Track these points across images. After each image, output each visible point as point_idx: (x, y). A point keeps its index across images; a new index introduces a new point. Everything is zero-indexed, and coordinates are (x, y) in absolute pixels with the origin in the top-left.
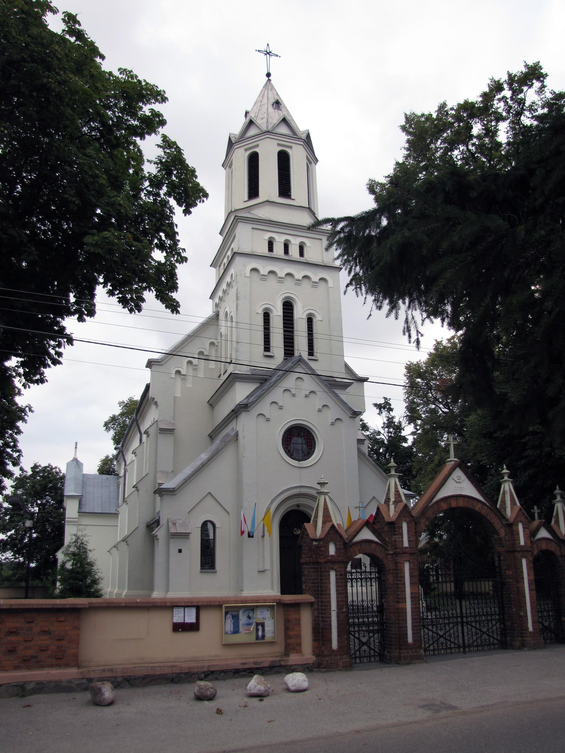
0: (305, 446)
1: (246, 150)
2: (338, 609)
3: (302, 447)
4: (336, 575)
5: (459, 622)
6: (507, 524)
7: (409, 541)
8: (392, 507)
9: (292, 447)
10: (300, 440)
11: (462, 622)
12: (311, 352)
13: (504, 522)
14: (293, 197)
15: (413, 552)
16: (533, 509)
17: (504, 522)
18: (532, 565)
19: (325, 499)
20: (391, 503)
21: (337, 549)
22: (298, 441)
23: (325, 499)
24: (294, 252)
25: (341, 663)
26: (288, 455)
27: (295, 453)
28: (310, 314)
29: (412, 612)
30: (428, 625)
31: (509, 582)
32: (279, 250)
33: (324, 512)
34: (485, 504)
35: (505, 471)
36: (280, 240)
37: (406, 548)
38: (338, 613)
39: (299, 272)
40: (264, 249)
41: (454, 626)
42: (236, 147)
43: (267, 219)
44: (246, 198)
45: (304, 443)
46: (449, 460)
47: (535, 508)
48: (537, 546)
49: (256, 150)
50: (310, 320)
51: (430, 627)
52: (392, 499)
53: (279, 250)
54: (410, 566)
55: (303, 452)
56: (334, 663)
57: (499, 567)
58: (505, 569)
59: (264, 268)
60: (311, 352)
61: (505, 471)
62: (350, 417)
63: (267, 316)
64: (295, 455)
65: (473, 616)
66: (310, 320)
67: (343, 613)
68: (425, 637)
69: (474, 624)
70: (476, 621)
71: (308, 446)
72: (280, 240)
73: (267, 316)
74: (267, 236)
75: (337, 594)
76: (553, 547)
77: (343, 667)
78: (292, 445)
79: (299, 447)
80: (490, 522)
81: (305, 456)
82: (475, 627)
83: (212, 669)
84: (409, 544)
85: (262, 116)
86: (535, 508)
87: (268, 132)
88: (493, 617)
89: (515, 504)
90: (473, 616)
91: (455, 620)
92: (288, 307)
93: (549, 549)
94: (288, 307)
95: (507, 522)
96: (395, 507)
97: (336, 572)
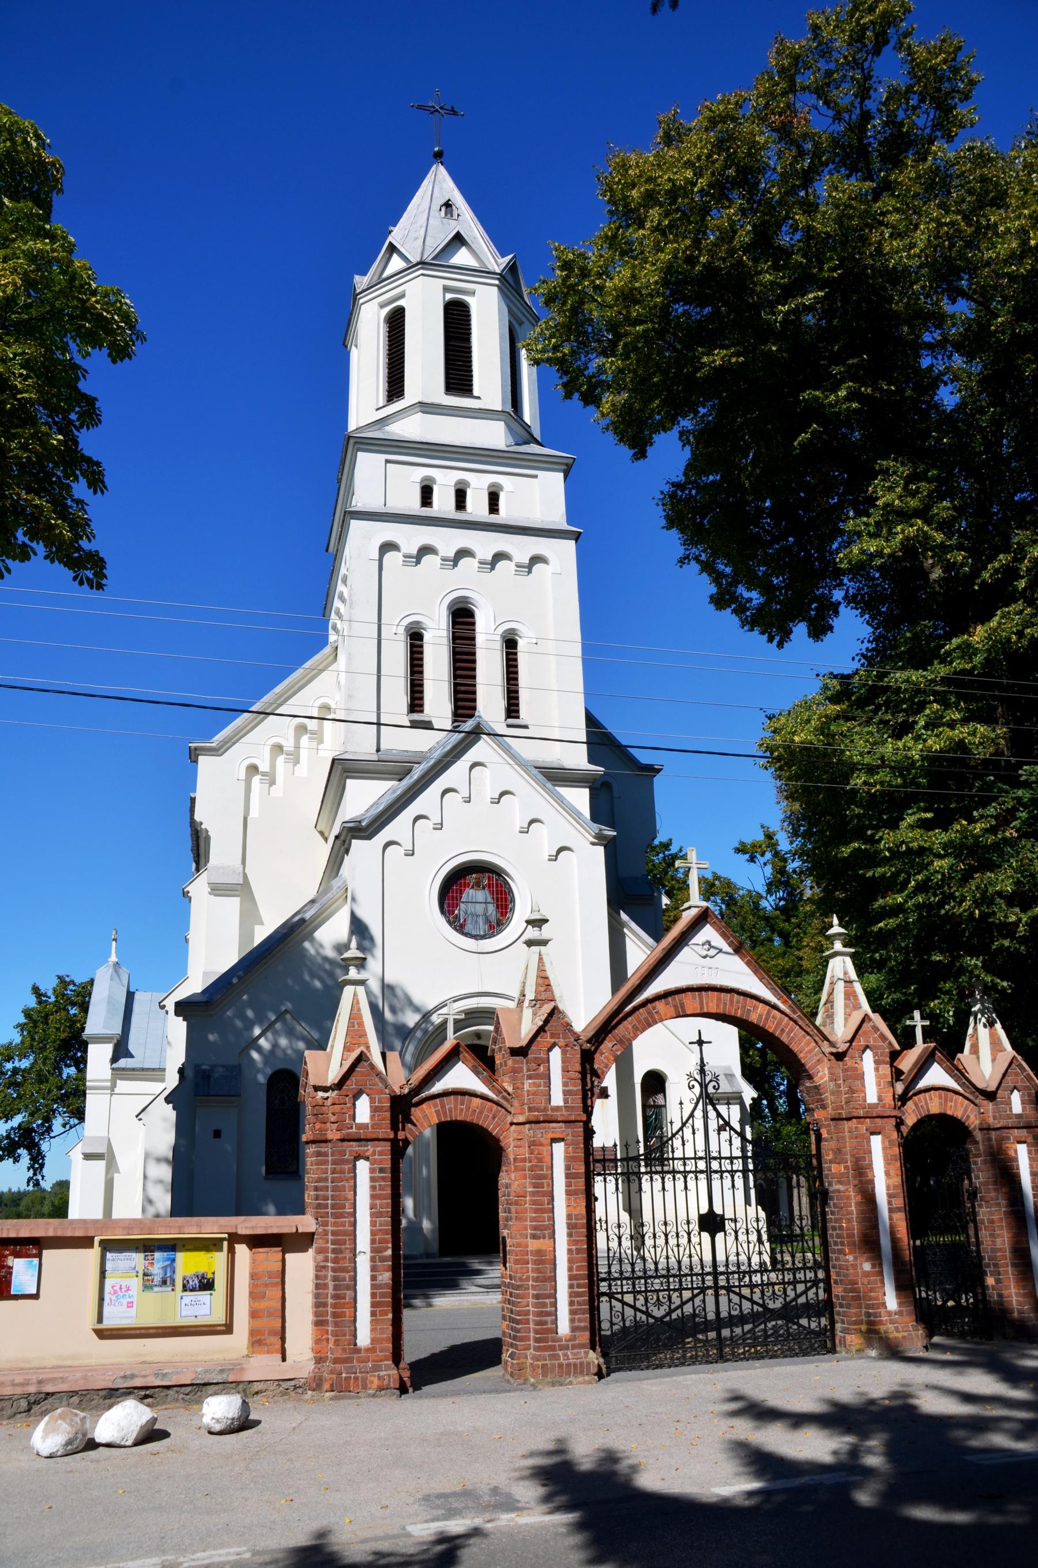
0: (491, 909)
1: (382, 306)
2: (373, 1250)
3: (486, 909)
4: (372, 1171)
5: (820, 1281)
6: (832, 1054)
7: (565, 1093)
8: (527, 1013)
9: (462, 910)
10: (480, 895)
11: (716, 1288)
12: (512, 709)
13: (827, 1049)
14: (476, 393)
15: (573, 1118)
16: (912, 1018)
17: (827, 1049)
18: (896, 1150)
19: (355, 995)
20: (526, 1003)
21: (374, 1110)
22: (476, 899)
23: (355, 995)
24: (477, 506)
25: (376, 1380)
26: (455, 929)
27: (469, 921)
28: (512, 631)
29: (570, 1261)
30: (622, 1293)
31: (839, 1191)
32: (443, 503)
33: (351, 1024)
34: (775, 1007)
35: (836, 929)
36: (445, 482)
37: (557, 1109)
38: (373, 1259)
39: (485, 544)
40: (412, 504)
41: (807, 1289)
42: (361, 301)
43: (418, 439)
44: (382, 399)
45: (489, 900)
46: (686, 905)
47: (917, 1014)
48: (916, 1105)
49: (401, 303)
50: (510, 644)
51: (629, 1298)
52: (530, 995)
53: (443, 503)
54: (566, 1152)
55: (487, 920)
56: (356, 1379)
57: (819, 1155)
58: (831, 1162)
59: (410, 538)
60: (512, 709)
61: (836, 929)
62: (593, 844)
63: (415, 638)
64: (468, 928)
65: (810, 1268)
66: (510, 644)
67: (383, 1259)
68: (615, 1320)
69: (629, 1298)
70: (635, 1292)
71: (497, 907)
72: (445, 482)
73: (415, 638)
74: (419, 474)
75: (372, 1215)
76: (959, 1109)
77: (381, 1389)
78: (462, 906)
79: (480, 909)
80: (791, 1051)
81: (491, 927)
82: (634, 1307)
83: (49, 1388)
84: (566, 1101)
85: (416, 235)
86: (917, 1014)
87: (422, 264)
88: (800, 1276)
89: (857, 1007)
90: (789, 1270)
91: (810, 1275)
92: (462, 616)
93: (949, 1112)
94: (462, 616)
95: (834, 1050)
96: (535, 1014)
97: (371, 1164)
